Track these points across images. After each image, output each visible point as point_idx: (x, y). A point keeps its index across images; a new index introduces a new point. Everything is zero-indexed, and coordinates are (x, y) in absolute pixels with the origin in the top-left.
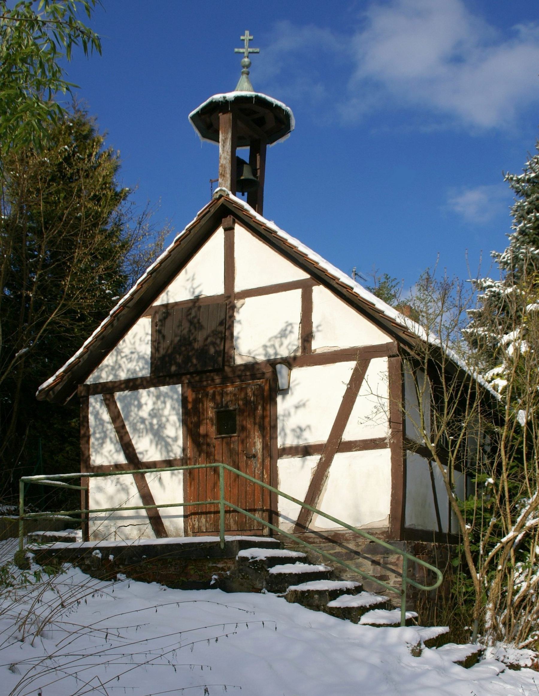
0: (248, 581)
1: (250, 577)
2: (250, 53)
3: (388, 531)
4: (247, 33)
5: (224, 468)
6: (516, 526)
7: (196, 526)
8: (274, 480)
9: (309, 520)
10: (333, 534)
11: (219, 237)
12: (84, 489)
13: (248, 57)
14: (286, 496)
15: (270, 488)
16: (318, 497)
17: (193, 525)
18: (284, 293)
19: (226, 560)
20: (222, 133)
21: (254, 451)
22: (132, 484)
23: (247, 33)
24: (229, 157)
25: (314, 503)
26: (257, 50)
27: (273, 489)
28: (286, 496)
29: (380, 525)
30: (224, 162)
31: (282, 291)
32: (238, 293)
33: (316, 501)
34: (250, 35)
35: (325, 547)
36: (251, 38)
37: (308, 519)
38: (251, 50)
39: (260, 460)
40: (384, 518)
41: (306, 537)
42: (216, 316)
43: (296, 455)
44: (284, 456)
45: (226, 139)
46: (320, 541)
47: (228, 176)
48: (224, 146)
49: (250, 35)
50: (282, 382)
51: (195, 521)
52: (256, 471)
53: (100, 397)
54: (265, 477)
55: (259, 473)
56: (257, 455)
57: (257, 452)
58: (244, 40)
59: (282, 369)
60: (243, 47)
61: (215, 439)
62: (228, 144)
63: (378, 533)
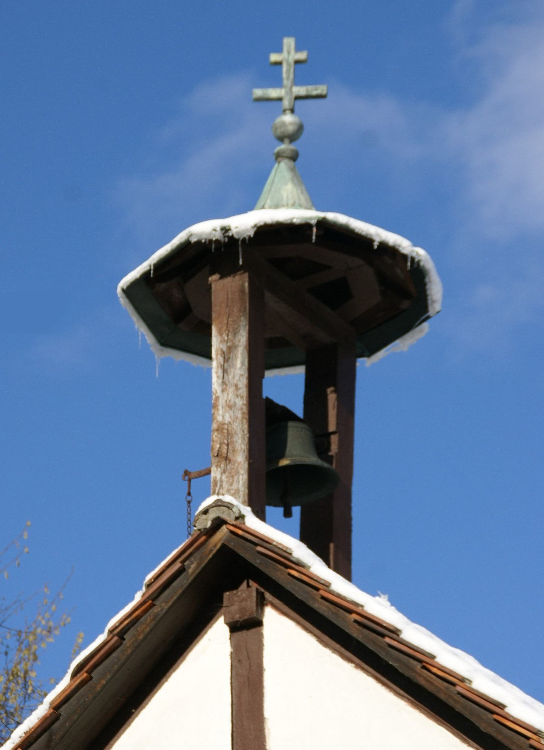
2: (298, 98)
4: (289, 42)
13: (292, 111)
20: (220, 333)
23: (289, 42)
26: (321, 89)
30: (227, 419)
34: (298, 49)
36: (302, 56)
38: (301, 90)
45: (231, 349)
49: (298, 49)
58: (279, 64)
62: (238, 364)
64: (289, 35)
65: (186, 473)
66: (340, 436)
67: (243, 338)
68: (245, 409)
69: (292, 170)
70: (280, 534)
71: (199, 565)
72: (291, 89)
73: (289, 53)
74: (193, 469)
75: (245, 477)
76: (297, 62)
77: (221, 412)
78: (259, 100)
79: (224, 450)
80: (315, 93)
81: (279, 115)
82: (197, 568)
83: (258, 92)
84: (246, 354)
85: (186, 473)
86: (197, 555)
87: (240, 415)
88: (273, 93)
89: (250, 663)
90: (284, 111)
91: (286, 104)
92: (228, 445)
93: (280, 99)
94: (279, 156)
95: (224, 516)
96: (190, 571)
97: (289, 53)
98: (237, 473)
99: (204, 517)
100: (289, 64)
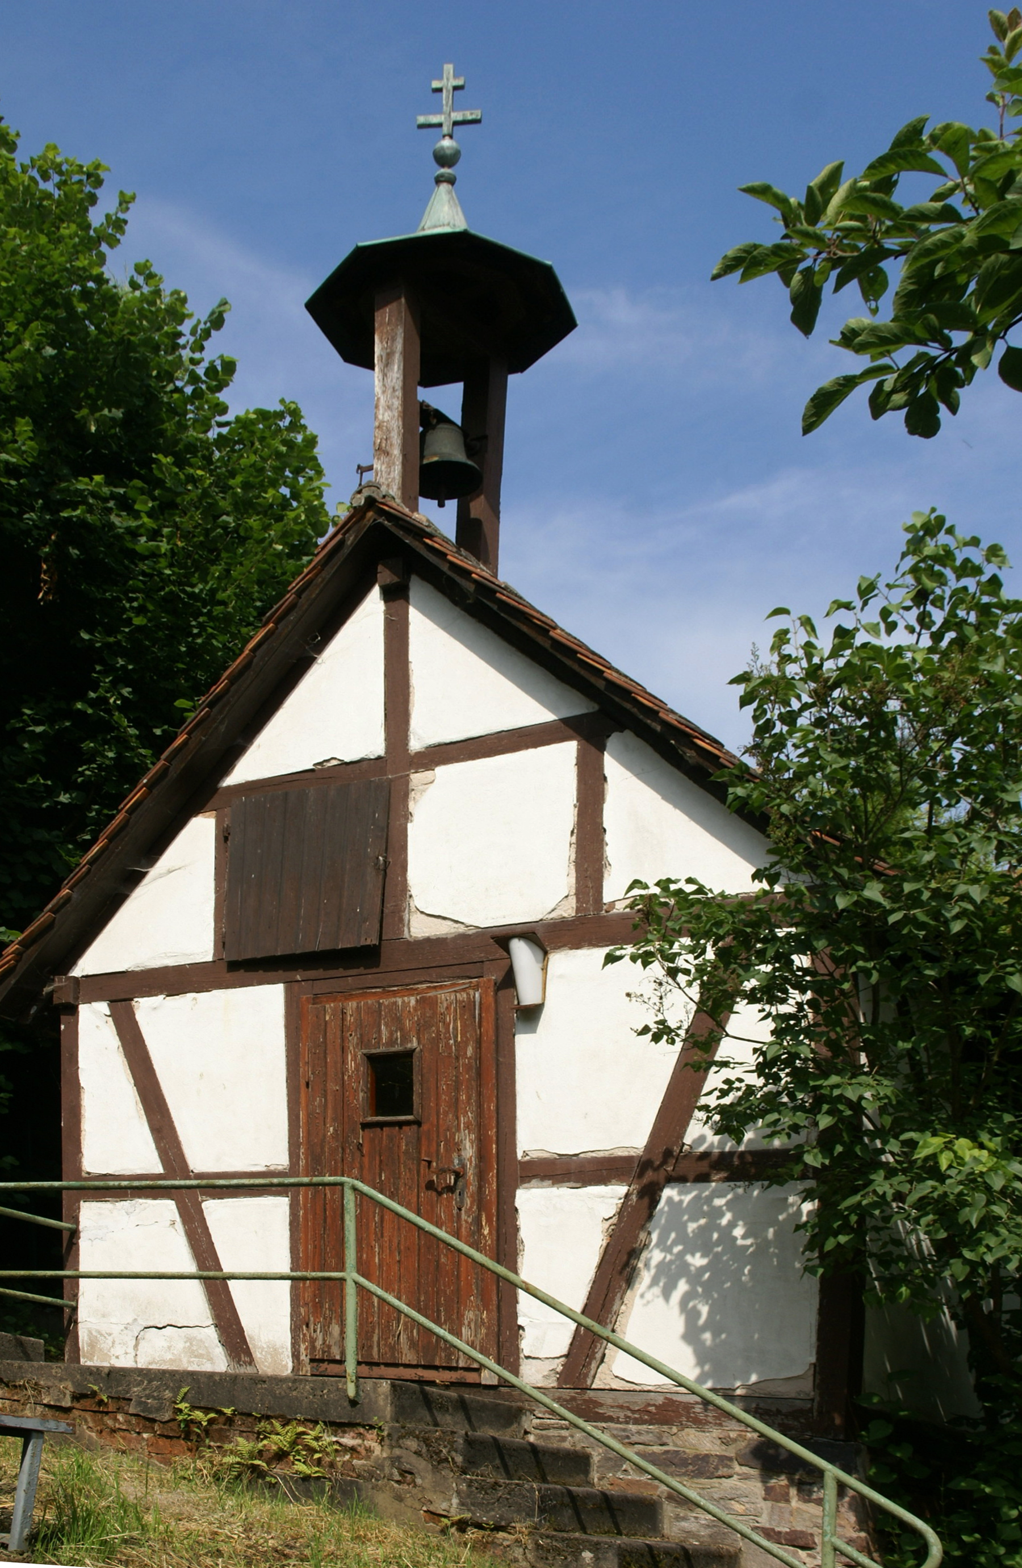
0: (415, 1491)
1: (419, 1481)
2: (456, 123)
3: (811, 1410)
4: (449, 68)
5: (355, 1189)
6: (551, 650)
7: (319, 1344)
8: (506, 1245)
9: (598, 1356)
10: (660, 1400)
11: (373, 607)
12: (69, 1229)
13: (451, 137)
14: (529, 1290)
15: (501, 1269)
16: (622, 1298)
17: (313, 1341)
18: (531, 751)
19: (362, 1430)
20: (381, 341)
21: (456, 1161)
22: (173, 1223)
23: (449, 68)
24: (397, 403)
25: (609, 1311)
26: (476, 114)
27: (511, 1276)
28: (529, 1290)
29: (789, 1390)
30: (386, 417)
31: (527, 747)
32: (419, 754)
33: (615, 1308)
34: (456, 76)
35: (639, 1433)
36: (460, 82)
37: (594, 1353)
38: (457, 116)
39: (472, 1188)
40: (800, 1372)
41: (591, 1401)
42: (359, 809)
43: (563, 1182)
44: (534, 1182)
45: (390, 355)
46: (626, 1417)
47: (396, 452)
48: (385, 375)
49: (456, 76)
50: (528, 993)
51: (315, 1331)
52: (464, 1216)
53: (102, 1007)
54: (486, 1232)
55: (470, 1220)
56: (465, 1174)
57: (464, 1166)
58: (439, 90)
59: (522, 952)
60: (440, 111)
61: (365, 1126)
62: (396, 367)
63: (784, 1411)
64: (449, 62)
65: (359, 467)
66: (697, 1101)
67: (399, 346)
68: (400, 408)
69: (450, 192)
70: (440, 518)
71: (356, 536)
72: (450, 115)
73: (448, 79)
74: (364, 464)
75: (400, 467)
76: (456, 88)
77: (381, 411)
78: (421, 126)
79: (384, 445)
80: (470, 117)
81: (439, 140)
82: (354, 539)
83: (421, 119)
84: (401, 358)
85: (359, 467)
86: (355, 528)
87: (396, 415)
88: (434, 119)
89: (1002, 126)
90: (444, 136)
91: (445, 129)
92: (386, 440)
93: (440, 125)
94: (439, 180)
95: (374, 495)
96: (349, 543)
97: (448, 79)
98: (394, 464)
99: (359, 496)
100: (448, 91)
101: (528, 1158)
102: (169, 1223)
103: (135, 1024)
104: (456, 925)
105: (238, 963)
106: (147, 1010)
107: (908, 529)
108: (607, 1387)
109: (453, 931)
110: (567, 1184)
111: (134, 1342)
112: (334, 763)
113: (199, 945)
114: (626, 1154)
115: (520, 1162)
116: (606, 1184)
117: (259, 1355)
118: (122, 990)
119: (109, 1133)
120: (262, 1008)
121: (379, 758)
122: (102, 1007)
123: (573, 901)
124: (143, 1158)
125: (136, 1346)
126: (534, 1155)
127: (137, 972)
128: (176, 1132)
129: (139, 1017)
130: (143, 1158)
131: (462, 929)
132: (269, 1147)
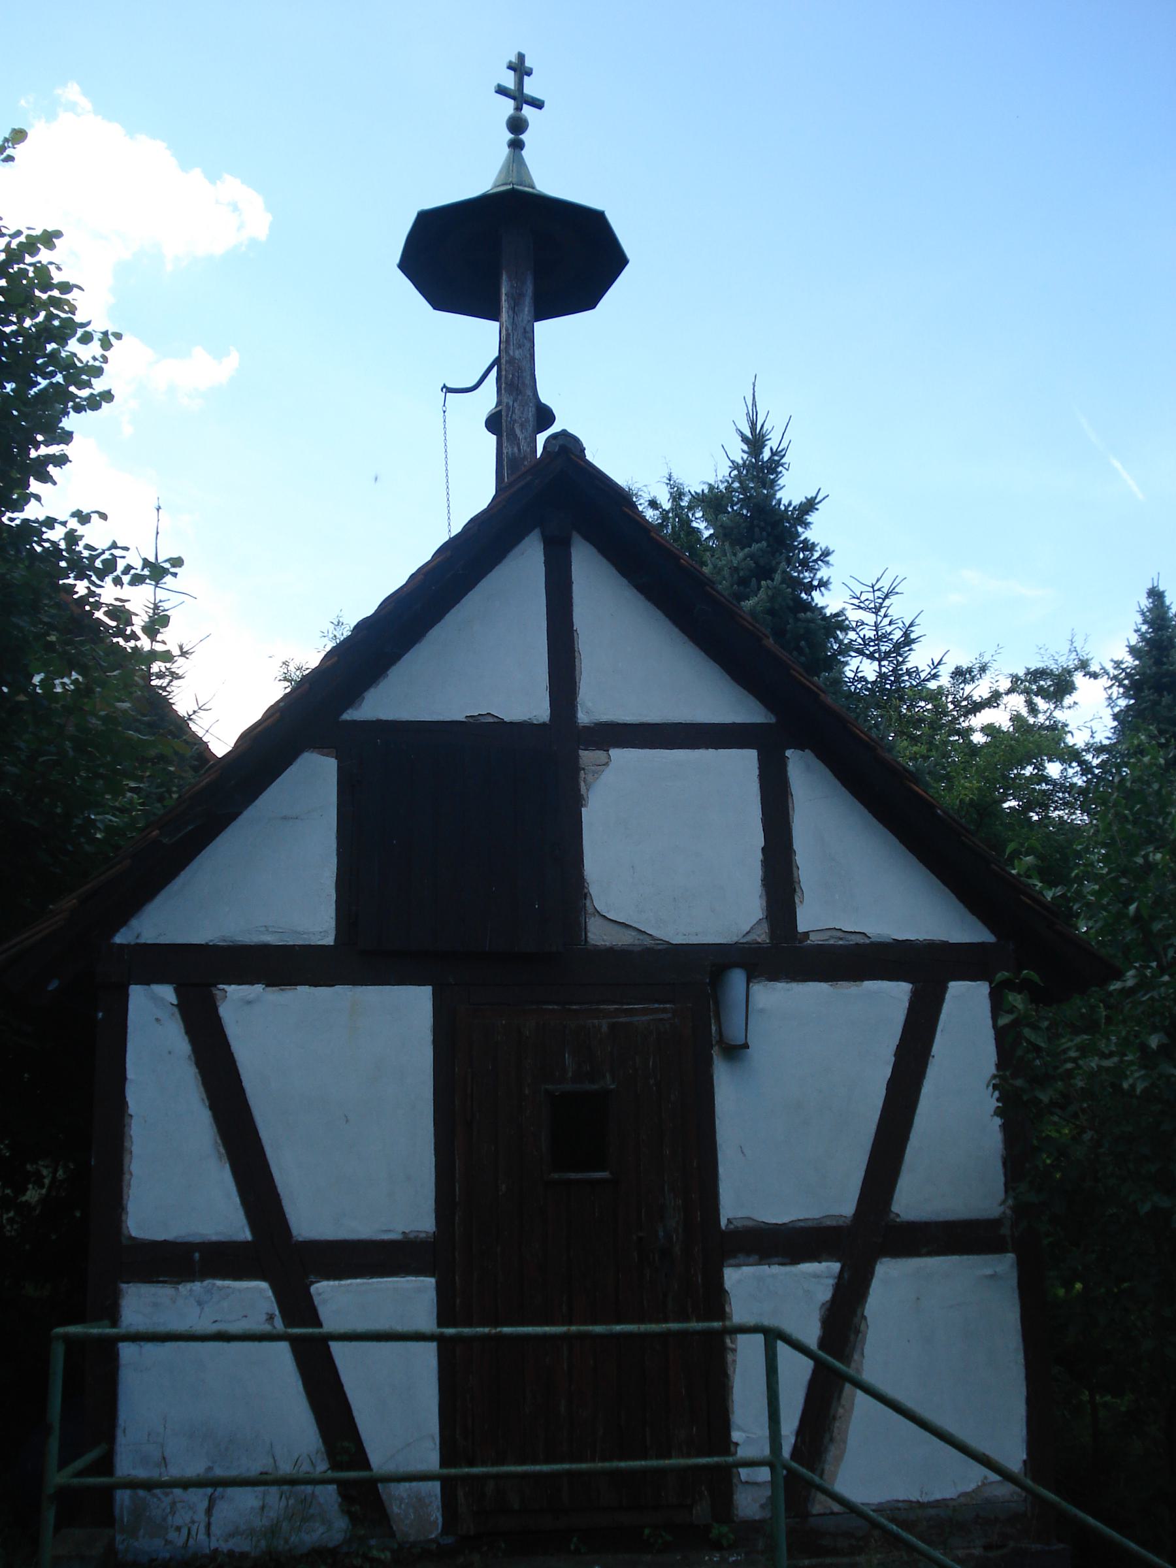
53: (167, 993)
65: (444, 386)
85: (444, 386)
101: (732, 1227)
102: (264, 1317)
103: (218, 1020)
104: (641, 937)
105: (362, 951)
106: (244, 1009)
107: (826, 553)
108: (828, 1511)
109: (637, 942)
110: (776, 1260)
111: (206, 1503)
112: (491, 720)
113: (313, 919)
114: (834, 1223)
115: (723, 1233)
116: (820, 1262)
117: (396, 1510)
118: (200, 975)
119: (173, 1182)
120: (403, 1018)
121: (544, 724)
122: (167, 993)
123: (765, 927)
124: (221, 1216)
125: (209, 1511)
126: (739, 1224)
127: (222, 947)
128: (273, 1180)
129: (226, 1012)
130: (221, 1216)
131: (648, 942)
132: (403, 1200)
